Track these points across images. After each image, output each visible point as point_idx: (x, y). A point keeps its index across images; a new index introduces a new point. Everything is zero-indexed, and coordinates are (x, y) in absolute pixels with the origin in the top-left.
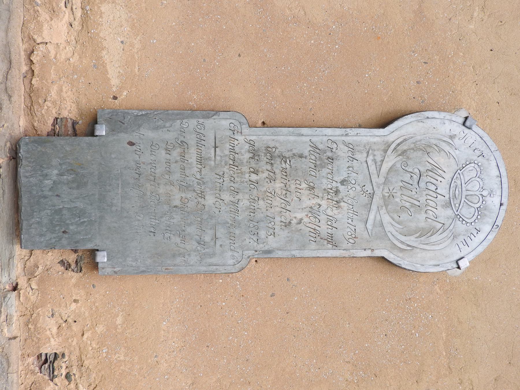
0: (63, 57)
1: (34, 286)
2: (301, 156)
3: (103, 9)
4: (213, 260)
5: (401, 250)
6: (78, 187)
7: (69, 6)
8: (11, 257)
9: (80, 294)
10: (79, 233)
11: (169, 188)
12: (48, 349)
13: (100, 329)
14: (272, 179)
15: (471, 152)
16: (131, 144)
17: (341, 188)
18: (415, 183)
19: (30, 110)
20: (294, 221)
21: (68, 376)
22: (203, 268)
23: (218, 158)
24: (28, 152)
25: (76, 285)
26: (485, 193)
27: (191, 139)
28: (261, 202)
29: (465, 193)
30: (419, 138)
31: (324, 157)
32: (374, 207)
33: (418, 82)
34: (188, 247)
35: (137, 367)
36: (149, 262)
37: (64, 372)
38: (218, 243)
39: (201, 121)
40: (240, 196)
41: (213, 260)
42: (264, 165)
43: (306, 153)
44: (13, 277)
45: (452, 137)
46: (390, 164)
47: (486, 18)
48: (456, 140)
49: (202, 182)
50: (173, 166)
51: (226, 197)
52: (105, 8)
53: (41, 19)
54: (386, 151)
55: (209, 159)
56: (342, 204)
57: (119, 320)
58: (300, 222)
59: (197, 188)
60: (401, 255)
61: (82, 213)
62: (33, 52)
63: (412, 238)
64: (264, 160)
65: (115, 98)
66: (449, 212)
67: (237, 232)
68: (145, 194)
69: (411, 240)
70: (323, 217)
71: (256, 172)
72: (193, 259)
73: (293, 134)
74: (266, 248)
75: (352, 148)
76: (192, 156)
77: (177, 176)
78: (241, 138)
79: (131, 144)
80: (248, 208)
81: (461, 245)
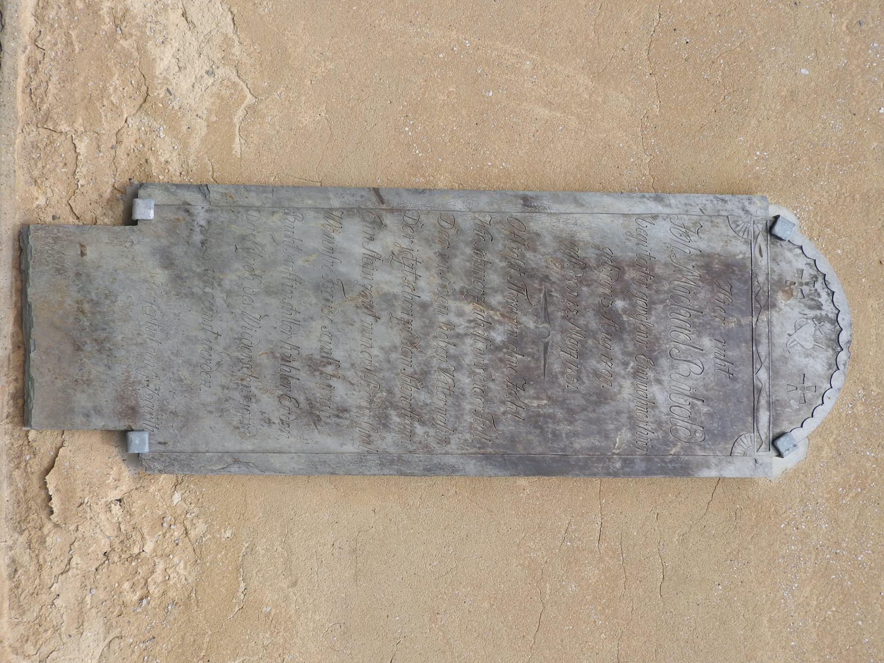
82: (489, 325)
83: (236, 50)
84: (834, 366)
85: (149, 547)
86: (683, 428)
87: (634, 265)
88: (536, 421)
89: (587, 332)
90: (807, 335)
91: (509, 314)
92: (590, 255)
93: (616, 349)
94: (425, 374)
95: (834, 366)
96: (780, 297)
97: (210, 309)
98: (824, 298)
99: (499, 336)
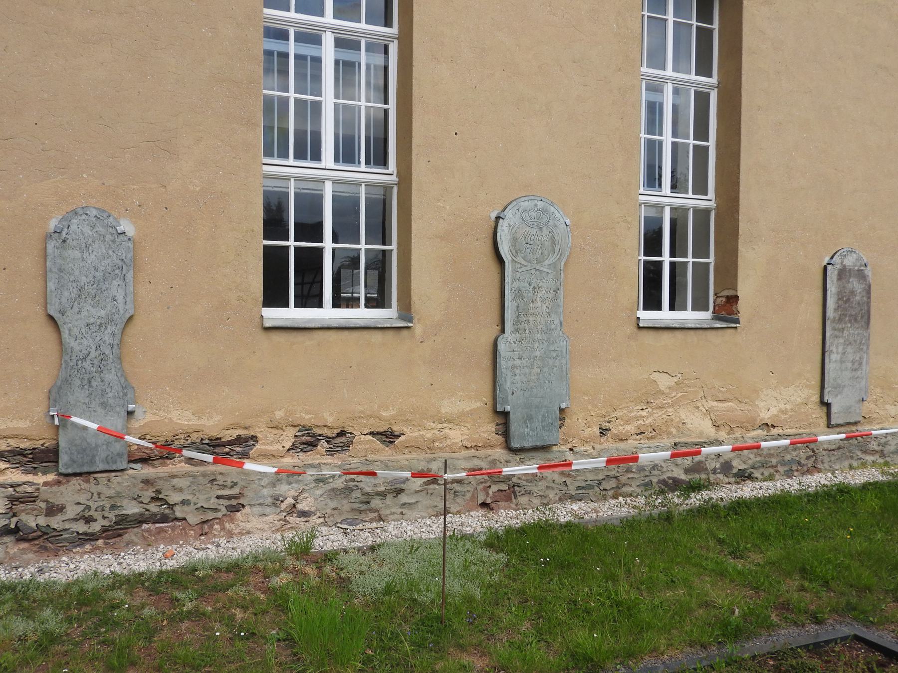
0: (467, 432)
1: (571, 440)
2: (518, 307)
3: (444, 412)
4: (564, 352)
5: (561, 255)
6: (533, 419)
7: (441, 430)
8: (559, 451)
9: (575, 418)
10: (552, 417)
11: (532, 374)
12: (598, 432)
13: (590, 407)
14: (528, 322)
15: (517, 216)
16: (513, 394)
17: (532, 286)
18: (531, 246)
19: (492, 447)
20: (547, 310)
21: (609, 422)
22: (568, 356)
23: (519, 350)
24: (518, 443)
25: (571, 420)
26: (536, 209)
27: (510, 363)
28: (539, 328)
29: (536, 220)
30: (510, 244)
31: (518, 294)
32: (541, 269)
33: (477, 240)
34: (558, 364)
35: (606, 388)
36: (564, 383)
37: (607, 424)
38: (557, 349)
39: (502, 358)
40: (536, 338)
41: (564, 352)
42: (522, 326)
43: (516, 304)
44: (568, 450)
45: (510, 226)
46: (522, 259)
47: (443, 199)
48: (511, 224)
49: (529, 358)
50: (522, 372)
51: (536, 345)
52: (443, 411)
53: (450, 443)
54: (516, 262)
55: (519, 354)
56: (540, 285)
57: (586, 398)
58: (547, 307)
59: (532, 360)
60: (563, 255)
61: (544, 416)
62: (466, 447)
63: (556, 249)
64: (519, 326)
65: (486, 404)
66: (544, 229)
67: (552, 339)
68: (535, 386)
69: (557, 249)
70: (546, 295)
71: (525, 330)
72: (563, 361)
73: (508, 312)
74: (559, 324)
75: (514, 279)
76: (517, 363)
77: (527, 371)
78: (510, 338)
79: (513, 394)
80: (541, 334)
81: (560, 223)
82: (848, 327)
83: (797, 384)
84: (855, 252)
85: (875, 397)
86: (864, 286)
87: (838, 296)
88: (862, 317)
89: (849, 306)
90: (850, 258)
91: (846, 323)
92: (837, 305)
93: (852, 300)
94: (855, 341)
95: (855, 252)
96: (844, 263)
97: (845, 386)
98: (844, 254)
99: (849, 325)
